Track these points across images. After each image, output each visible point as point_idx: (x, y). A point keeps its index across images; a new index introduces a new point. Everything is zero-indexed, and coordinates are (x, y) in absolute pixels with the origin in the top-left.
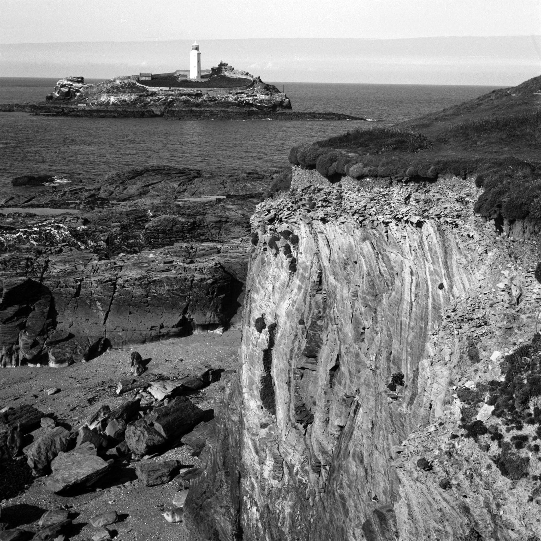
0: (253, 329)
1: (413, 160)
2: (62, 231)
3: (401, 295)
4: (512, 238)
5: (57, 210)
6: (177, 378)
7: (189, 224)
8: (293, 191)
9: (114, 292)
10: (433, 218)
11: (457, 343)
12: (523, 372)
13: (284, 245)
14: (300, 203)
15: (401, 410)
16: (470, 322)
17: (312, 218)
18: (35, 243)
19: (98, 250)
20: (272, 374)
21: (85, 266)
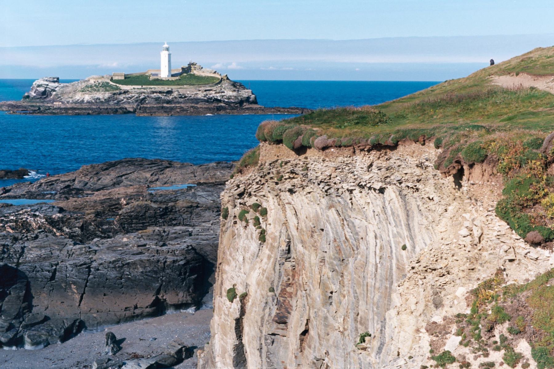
0: (225, 299)
1: (373, 133)
2: (38, 219)
3: (367, 258)
4: (472, 182)
5: (33, 200)
6: (151, 356)
7: (161, 209)
8: (261, 165)
9: (89, 275)
10: (395, 184)
11: (422, 293)
12: (487, 304)
13: (254, 217)
14: (268, 177)
15: (370, 360)
16: (433, 272)
17: (280, 190)
18: (11, 231)
19: (73, 236)
20: (243, 341)
21: (61, 250)
